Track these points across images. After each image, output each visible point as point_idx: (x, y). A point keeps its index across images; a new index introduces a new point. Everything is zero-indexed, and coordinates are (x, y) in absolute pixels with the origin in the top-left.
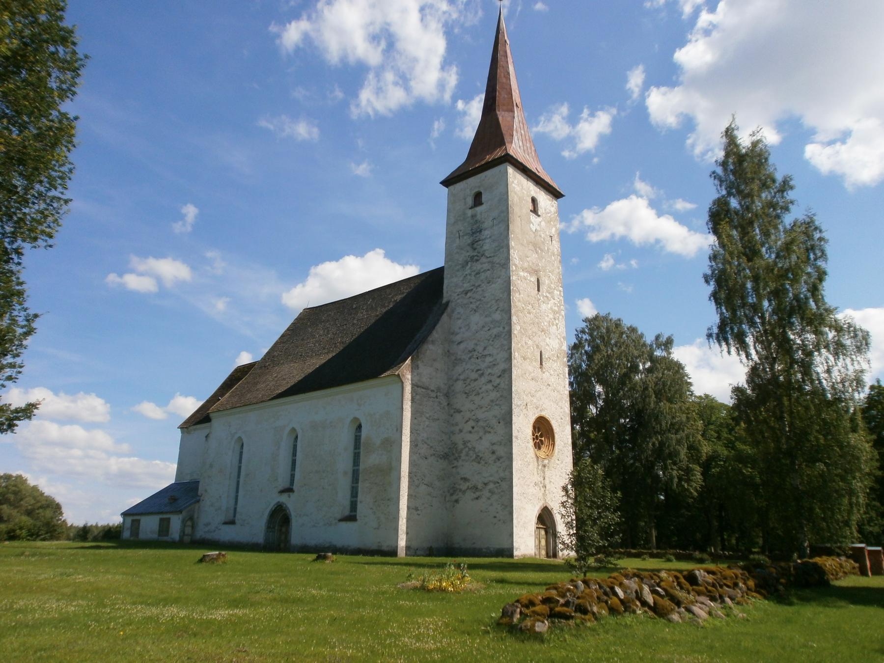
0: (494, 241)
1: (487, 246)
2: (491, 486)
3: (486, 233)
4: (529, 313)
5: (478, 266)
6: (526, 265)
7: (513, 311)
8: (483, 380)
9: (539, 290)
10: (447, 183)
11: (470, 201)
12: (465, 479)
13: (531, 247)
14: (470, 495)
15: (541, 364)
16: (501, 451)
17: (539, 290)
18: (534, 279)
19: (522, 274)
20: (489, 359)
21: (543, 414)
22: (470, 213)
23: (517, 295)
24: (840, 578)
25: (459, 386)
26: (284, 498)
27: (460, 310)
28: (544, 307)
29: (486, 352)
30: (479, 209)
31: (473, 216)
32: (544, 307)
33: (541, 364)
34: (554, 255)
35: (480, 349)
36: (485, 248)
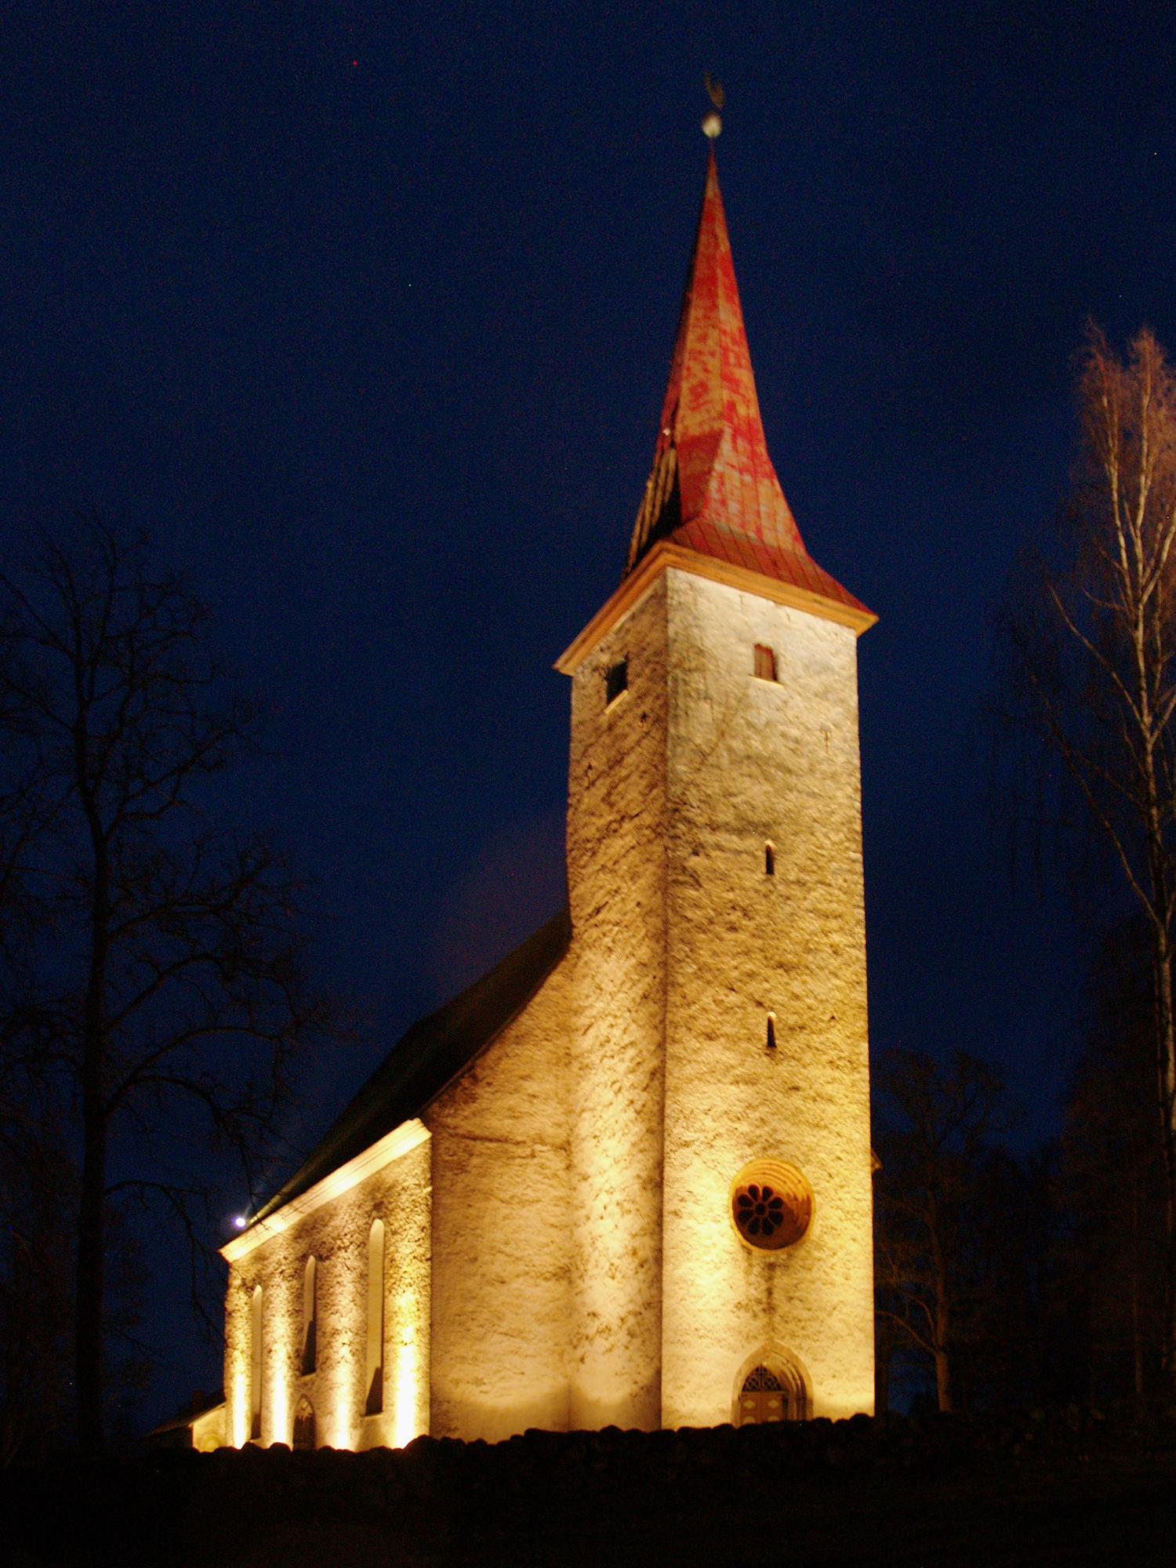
4: (733, 928)
9: (770, 870)
17: (770, 870)
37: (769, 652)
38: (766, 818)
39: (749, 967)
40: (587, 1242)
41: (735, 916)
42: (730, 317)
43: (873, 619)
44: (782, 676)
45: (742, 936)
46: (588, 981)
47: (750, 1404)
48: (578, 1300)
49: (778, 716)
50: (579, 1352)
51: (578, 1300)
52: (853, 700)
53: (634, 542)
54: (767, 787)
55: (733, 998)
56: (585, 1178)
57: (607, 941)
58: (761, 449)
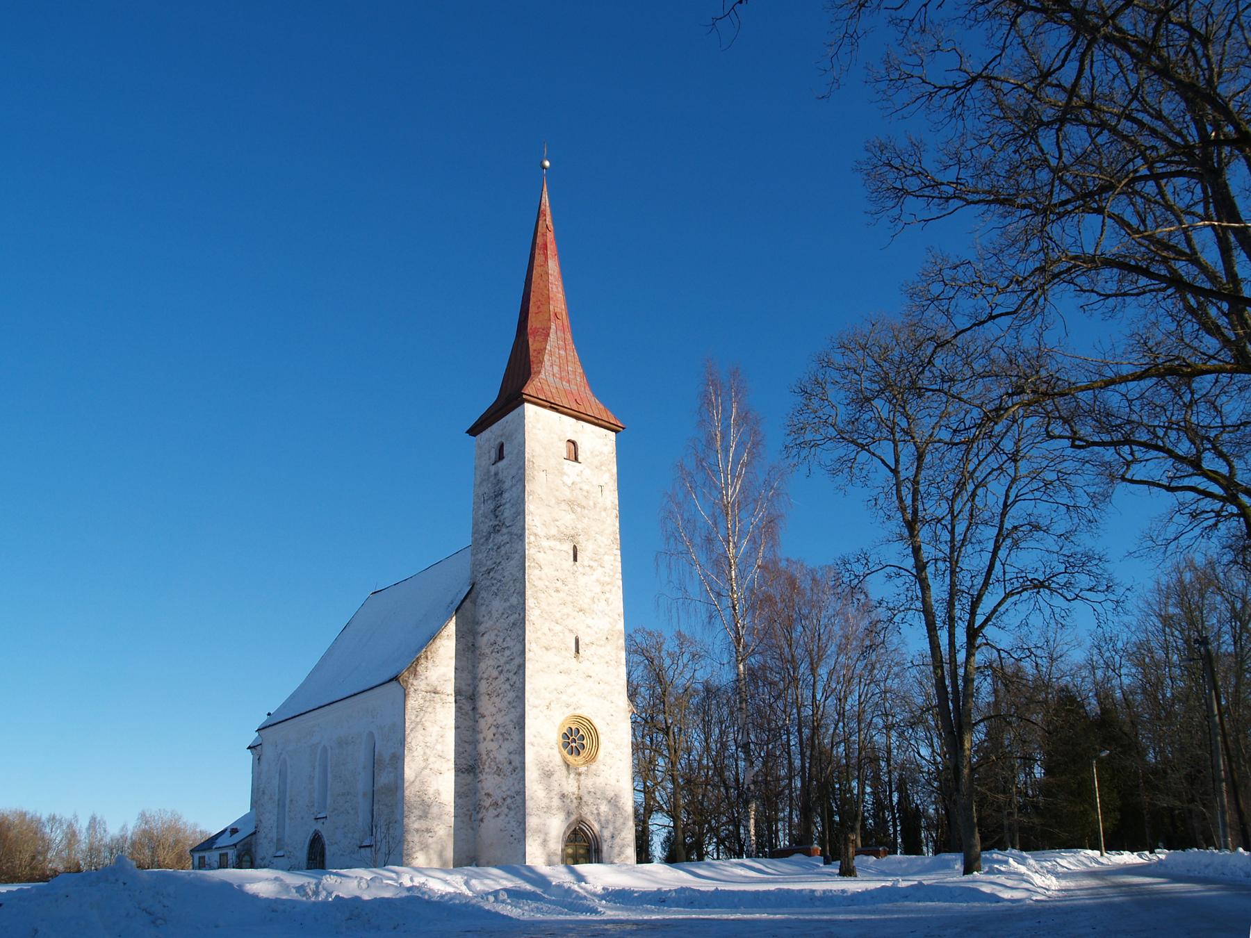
0: (512, 506)
1: (507, 513)
2: (509, 801)
3: (506, 495)
4: (557, 591)
5: (499, 539)
6: (554, 531)
7: (528, 593)
8: (502, 678)
9: (575, 559)
10: (474, 431)
11: (493, 455)
12: (488, 795)
13: (564, 506)
14: (492, 812)
15: (577, 651)
16: (516, 763)
17: (575, 559)
18: (965, 397)
19: (545, 543)
20: (507, 653)
21: (578, 712)
22: (493, 469)
23: (537, 572)
24: (692, 861)
25: (483, 687)
26: (318, 826)
27: (483, 594)
28: (582, 580)
29: (505, 645)
30: (501, 464)
31: (496, 474)
32: (582, 580)
33: (577, 651)
34: (605, 510)
35: (500, 640)
36: (506, 514)
37: (574, 443)
38: (573, 532)
39: (565, 611)
40: (484, 753)
41: (559, 584)
42: (1243, 256)
43: (839, 863)
44: (580, 459)
45: (561, 595)
46: (484, 608)
47: (570, 851)
48: (479, 785)
49: (578, 479)
50: (480, 816)
51: (479, 785)
52: (615, 470)
53: (553, 266)
54: (573, 516)
55: (558, 628)
56: (483, 716)
57: (494, 588)
58: (569, 336)
